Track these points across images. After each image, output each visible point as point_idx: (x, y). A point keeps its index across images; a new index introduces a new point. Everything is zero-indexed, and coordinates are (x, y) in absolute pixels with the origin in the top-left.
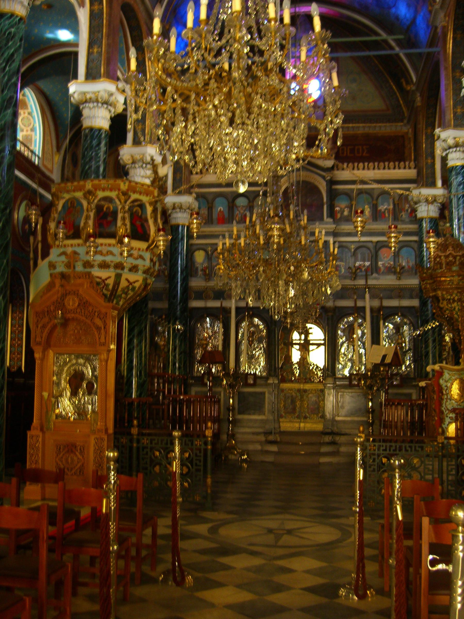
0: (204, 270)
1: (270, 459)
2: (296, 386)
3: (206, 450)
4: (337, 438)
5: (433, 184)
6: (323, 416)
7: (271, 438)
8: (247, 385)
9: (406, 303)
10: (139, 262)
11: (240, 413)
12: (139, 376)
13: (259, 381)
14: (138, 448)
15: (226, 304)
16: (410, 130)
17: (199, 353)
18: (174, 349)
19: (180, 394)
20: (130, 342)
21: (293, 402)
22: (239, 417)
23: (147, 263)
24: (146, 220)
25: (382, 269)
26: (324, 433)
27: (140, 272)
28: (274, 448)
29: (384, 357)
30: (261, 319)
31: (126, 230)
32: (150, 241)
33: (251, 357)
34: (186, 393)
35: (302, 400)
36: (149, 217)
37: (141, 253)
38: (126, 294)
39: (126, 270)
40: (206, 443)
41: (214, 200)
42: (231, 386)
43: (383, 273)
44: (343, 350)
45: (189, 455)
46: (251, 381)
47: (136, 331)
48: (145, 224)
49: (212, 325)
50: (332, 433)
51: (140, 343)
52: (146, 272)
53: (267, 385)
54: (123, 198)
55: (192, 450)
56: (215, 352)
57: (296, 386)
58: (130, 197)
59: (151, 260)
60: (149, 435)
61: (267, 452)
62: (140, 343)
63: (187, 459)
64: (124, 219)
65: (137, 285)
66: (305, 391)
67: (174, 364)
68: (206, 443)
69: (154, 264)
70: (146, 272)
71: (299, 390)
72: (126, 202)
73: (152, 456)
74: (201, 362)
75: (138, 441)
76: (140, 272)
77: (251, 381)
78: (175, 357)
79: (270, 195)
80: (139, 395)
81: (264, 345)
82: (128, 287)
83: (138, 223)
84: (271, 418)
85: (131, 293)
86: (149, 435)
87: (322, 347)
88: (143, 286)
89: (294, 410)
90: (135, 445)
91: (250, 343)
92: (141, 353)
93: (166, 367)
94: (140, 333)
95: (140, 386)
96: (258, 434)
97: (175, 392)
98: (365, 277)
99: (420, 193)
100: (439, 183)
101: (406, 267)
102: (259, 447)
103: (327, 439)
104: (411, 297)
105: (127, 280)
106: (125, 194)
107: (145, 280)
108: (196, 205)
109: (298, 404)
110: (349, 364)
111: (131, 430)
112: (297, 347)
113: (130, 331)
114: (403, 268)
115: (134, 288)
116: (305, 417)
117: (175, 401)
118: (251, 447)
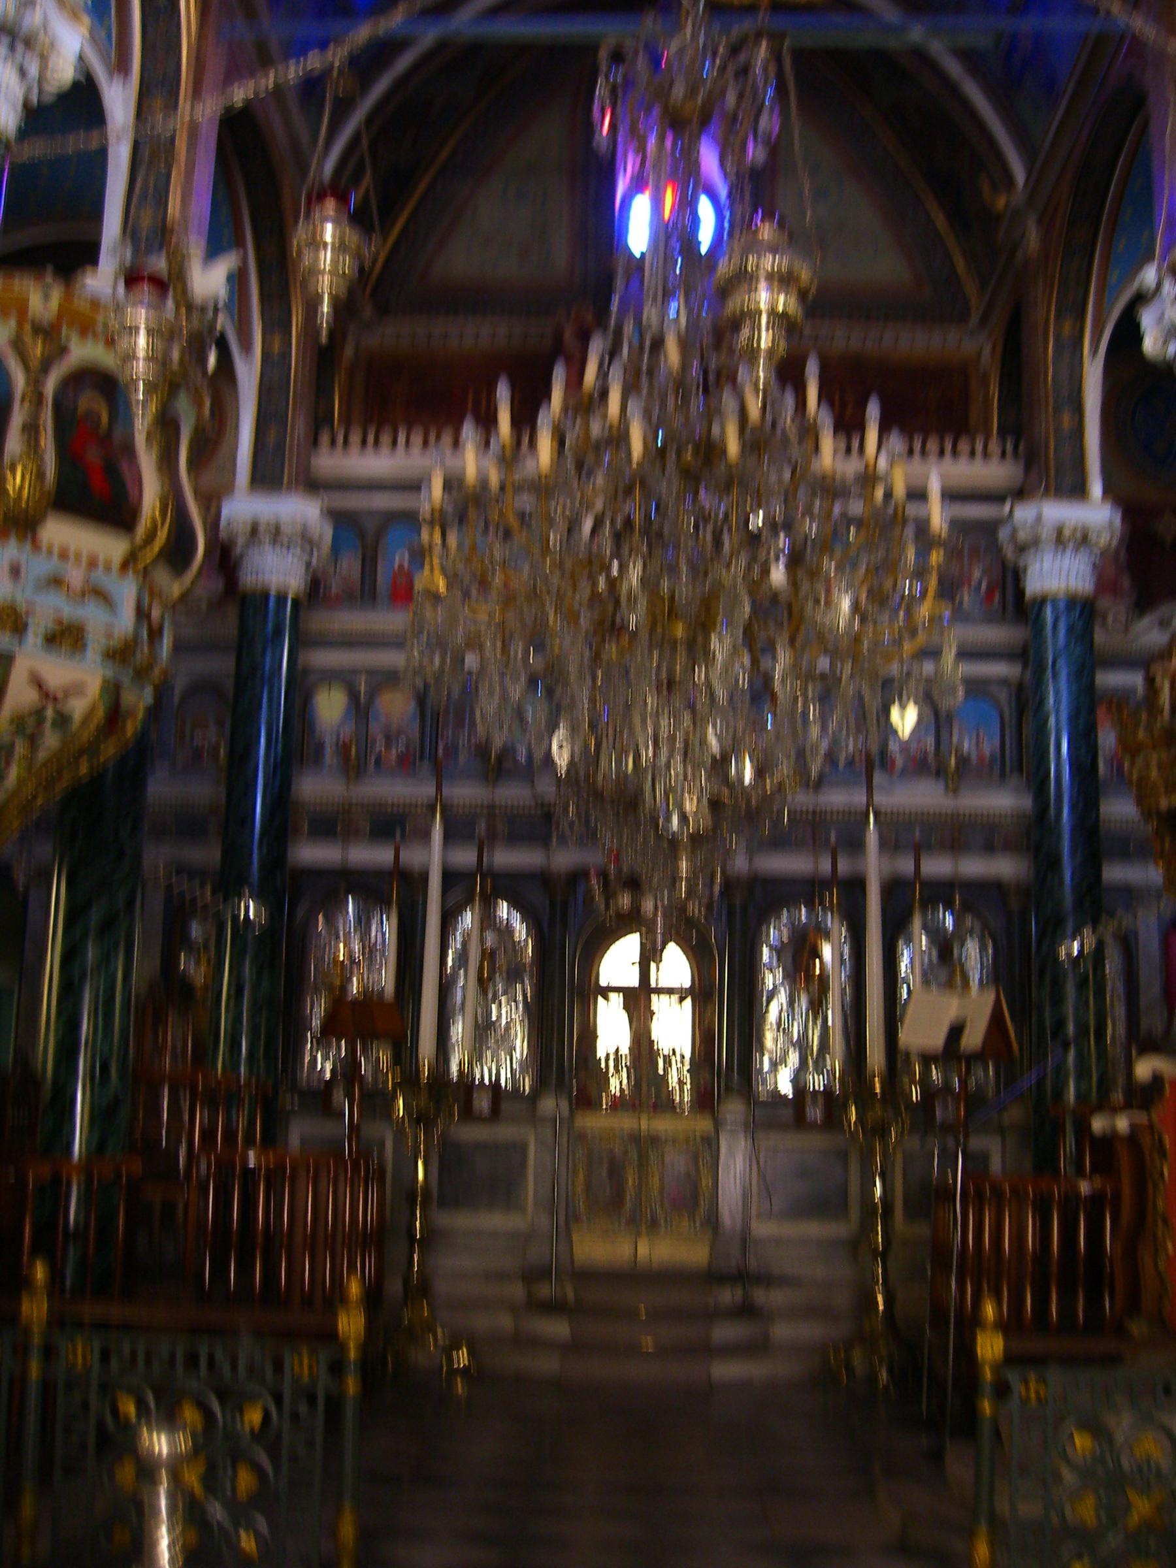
0: (343, 749)
1: (546, 1365)
2: (625, 1123)
3: (334, 1404)
4: (760, 1296)
5: (1079, 491)
6: (713, 1221)
7: (545, 1291)
8: (468, 1113)
9: (974, 867)
10: (92, 616)
11: (443, 1203)
12: (99, 1078)
13: (505, 1106)
14: (47, 1387)
15: (412, 857)
16: (987, 351)
17: (317, 1011)
18: (237, 991)
19: (249, 1141)
20: (70, 956)
21: (616, 1172)
22: (446, 1219)
23: (126, 620)
24: (129, 450)
25: (899, 762)
26: (713, 1277)
27: (93, 653)
28: (558, 1328)
29: (956, 1031)
30: (515, 904)
31: (41, 475)
32: (141, 530)
33: (484, 1030)
34: (271, 1138)
35: (643, 1164)
36: (140, 439)
37: (99, 575)
38: (33, 741)
39: (33, 639)
40: (337, 1368)
41: (379, 534)
42: (419, 1118)
43: (903, 772)
44: (773, 1012)
45: (266, 1417)
46: (482, 1103)
47: (95, 917)
48: (124, 467)
49: (363, 923)
50: (742, 1277)
51: (106, 959)
52: (119, 654)
53: (533, 1117)
54: (37, 350)
55: (278, 1399)
56: (370, 1001)
57: (625, 1123)
58: (63, 350)
59: (142, 613)
60: (101, 1326)
61: (534, 1343)
62: (106, 959)
63: (256, 1436)
64: (31, 430)
65: (78, 707)
66: (654, 1140)
67: (234, 1044)
68: (337, 1368)
69: (155, 634)
70: (119, 654)
71: (635, 1138)
72: (46, 366)
73: (109, 1419)
74: (331, 1029)
75: (49, 1352)
76: (93, 653)
77: (482, 1103)
78: (236, 1020)
79: (141, 1405)
80: (98, 1146)
81: (524, 989)
82: (39, 713)
83: (93, 455)
84: (544, 1221)
85: (51, 740)
86: (101, 1326)
87: (688, 1002)
88: (100, 713)
89: (617, 1199)
90: (35, 1369)
91: (483, 984)
92: (110, 1000)
93: (203, 1054)
94: (108, 926)
95: (100, 1116)
96: (500, 1276)
97: (230, 1135)
98: (864, 779)
99: (1039, 518)
100: (1096, 488)
101: (974, 757)
102: (505, 1322)
103: (727, 1296)
104: (989, 848)
105: (38, 682)
106: (49, 332)
107: (112, 690)
108: (324, 532)
109: (631, 1181)
110: (794, 1058)
111: (19, 1304)
112: (616, 999)
113: (74, 916)
114: (963, 761)
115: (63, 720)
116: (654, 1224)
117: (225, 1172)
118: (481, 1322)
